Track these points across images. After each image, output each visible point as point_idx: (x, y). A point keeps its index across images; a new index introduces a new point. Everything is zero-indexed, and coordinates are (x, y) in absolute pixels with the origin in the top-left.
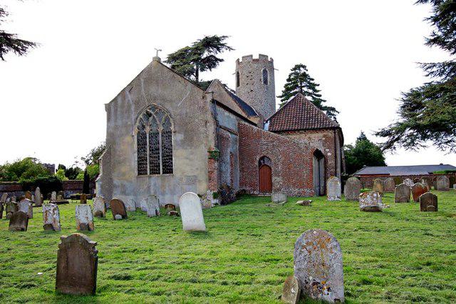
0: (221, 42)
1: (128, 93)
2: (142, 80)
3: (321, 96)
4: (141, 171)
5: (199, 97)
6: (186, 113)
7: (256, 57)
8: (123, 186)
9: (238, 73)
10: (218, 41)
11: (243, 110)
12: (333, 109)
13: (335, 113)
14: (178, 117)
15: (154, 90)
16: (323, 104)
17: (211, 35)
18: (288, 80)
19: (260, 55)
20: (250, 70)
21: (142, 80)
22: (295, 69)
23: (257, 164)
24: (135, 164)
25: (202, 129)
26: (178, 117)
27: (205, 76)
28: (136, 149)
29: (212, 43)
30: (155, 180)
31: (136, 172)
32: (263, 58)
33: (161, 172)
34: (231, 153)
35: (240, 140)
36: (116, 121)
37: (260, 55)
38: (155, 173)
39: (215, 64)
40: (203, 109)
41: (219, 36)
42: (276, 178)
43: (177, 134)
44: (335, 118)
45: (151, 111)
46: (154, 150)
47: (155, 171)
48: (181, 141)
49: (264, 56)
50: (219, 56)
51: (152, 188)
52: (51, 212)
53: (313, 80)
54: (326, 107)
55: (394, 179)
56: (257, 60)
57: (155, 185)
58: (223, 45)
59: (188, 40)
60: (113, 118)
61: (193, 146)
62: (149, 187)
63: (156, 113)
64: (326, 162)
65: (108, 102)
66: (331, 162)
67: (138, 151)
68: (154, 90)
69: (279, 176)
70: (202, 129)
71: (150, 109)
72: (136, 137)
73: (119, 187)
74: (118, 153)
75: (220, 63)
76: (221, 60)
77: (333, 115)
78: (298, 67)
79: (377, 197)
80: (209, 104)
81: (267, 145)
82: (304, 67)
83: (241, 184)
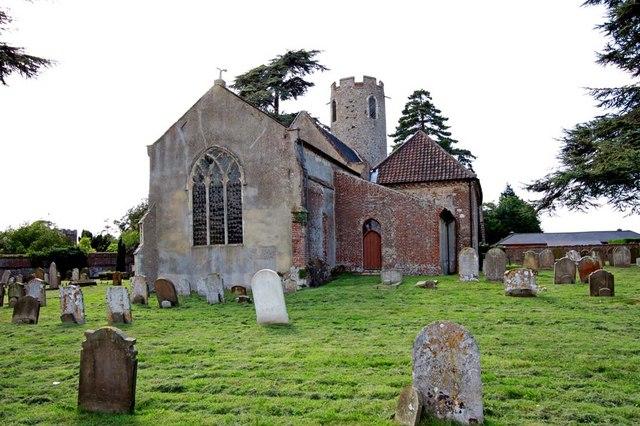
0: (311, 59)
1: (179, 130)
2: (200, 112)
3: (450, 134)
4: (198, 240)
5: (280, 136)
6: (262, 159)
7: (359, 79)
8: (173, 260)
9: (334, 102)
10: (306, 58)
11: (341, 155)
12: (468, 153)
13: (471, 159)
14: (250, 164)
15: (216, 126)
16: (454, 146)
17: (296, 49)
18: (405, 112)
19: (365, 77)
20: (351, 98)
21: (200, 112)
22: (413, 97)
23: (360, 229)
24: (189, 230)
25: (284, 181)
26: (250, 164)
27: (287, 107)
28: (191, 209)
29: (298, 60)
30: (218, 253)
31: (191, 241)
32: (369, 81)
33: (208, 243)
34: (324, 214)
35: (337, 197)
36: (162, 170)
37: (365, 77)
38: (217, 243)
39: (301, 90)
40: (284, 153)
41: (307, 50)
42: (387, 249)
43: (249, 188)
44: (470, 165)
45: (211, 156)
46: (217, 211)
47: (217, 239)
48: (254, 197)
49: (371, 78)
50: (307, 78)
51: (213, 263)
52: (72, 297)
53: (439, 112)
54: (457, 150)
55: (553, 251)
56: (361, 84)
57: (218, 259)
58: (313, 63)
59: (264, 56)
60: (158, 165)
61: (270, 204)
62: (209, 262)
63: (220, 159)
64: (457, 227)
65: (151, 143)
66: (464, 227)
67: (194, 212)
68: (216, 126)
69: (391, 247)
70: (284, 181)
71: (211, 153)
72: (190, 192)
73: (166, 262)
74: (166, 214)
75: (309, 88)
76: (311, 85)
77: (468, 161)
78: (418, 94)
79: (529, 277)
80: (293, 145)
81: (374, 203)
82: (427, 94)
83: (339, 258)
